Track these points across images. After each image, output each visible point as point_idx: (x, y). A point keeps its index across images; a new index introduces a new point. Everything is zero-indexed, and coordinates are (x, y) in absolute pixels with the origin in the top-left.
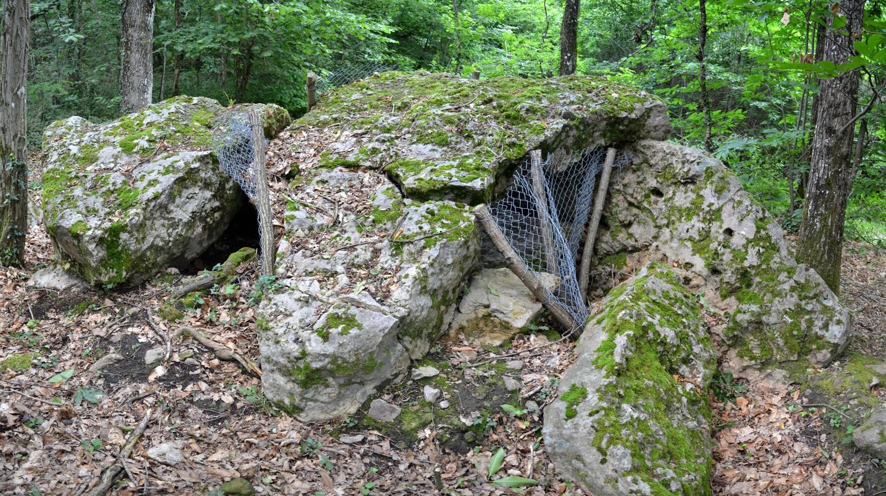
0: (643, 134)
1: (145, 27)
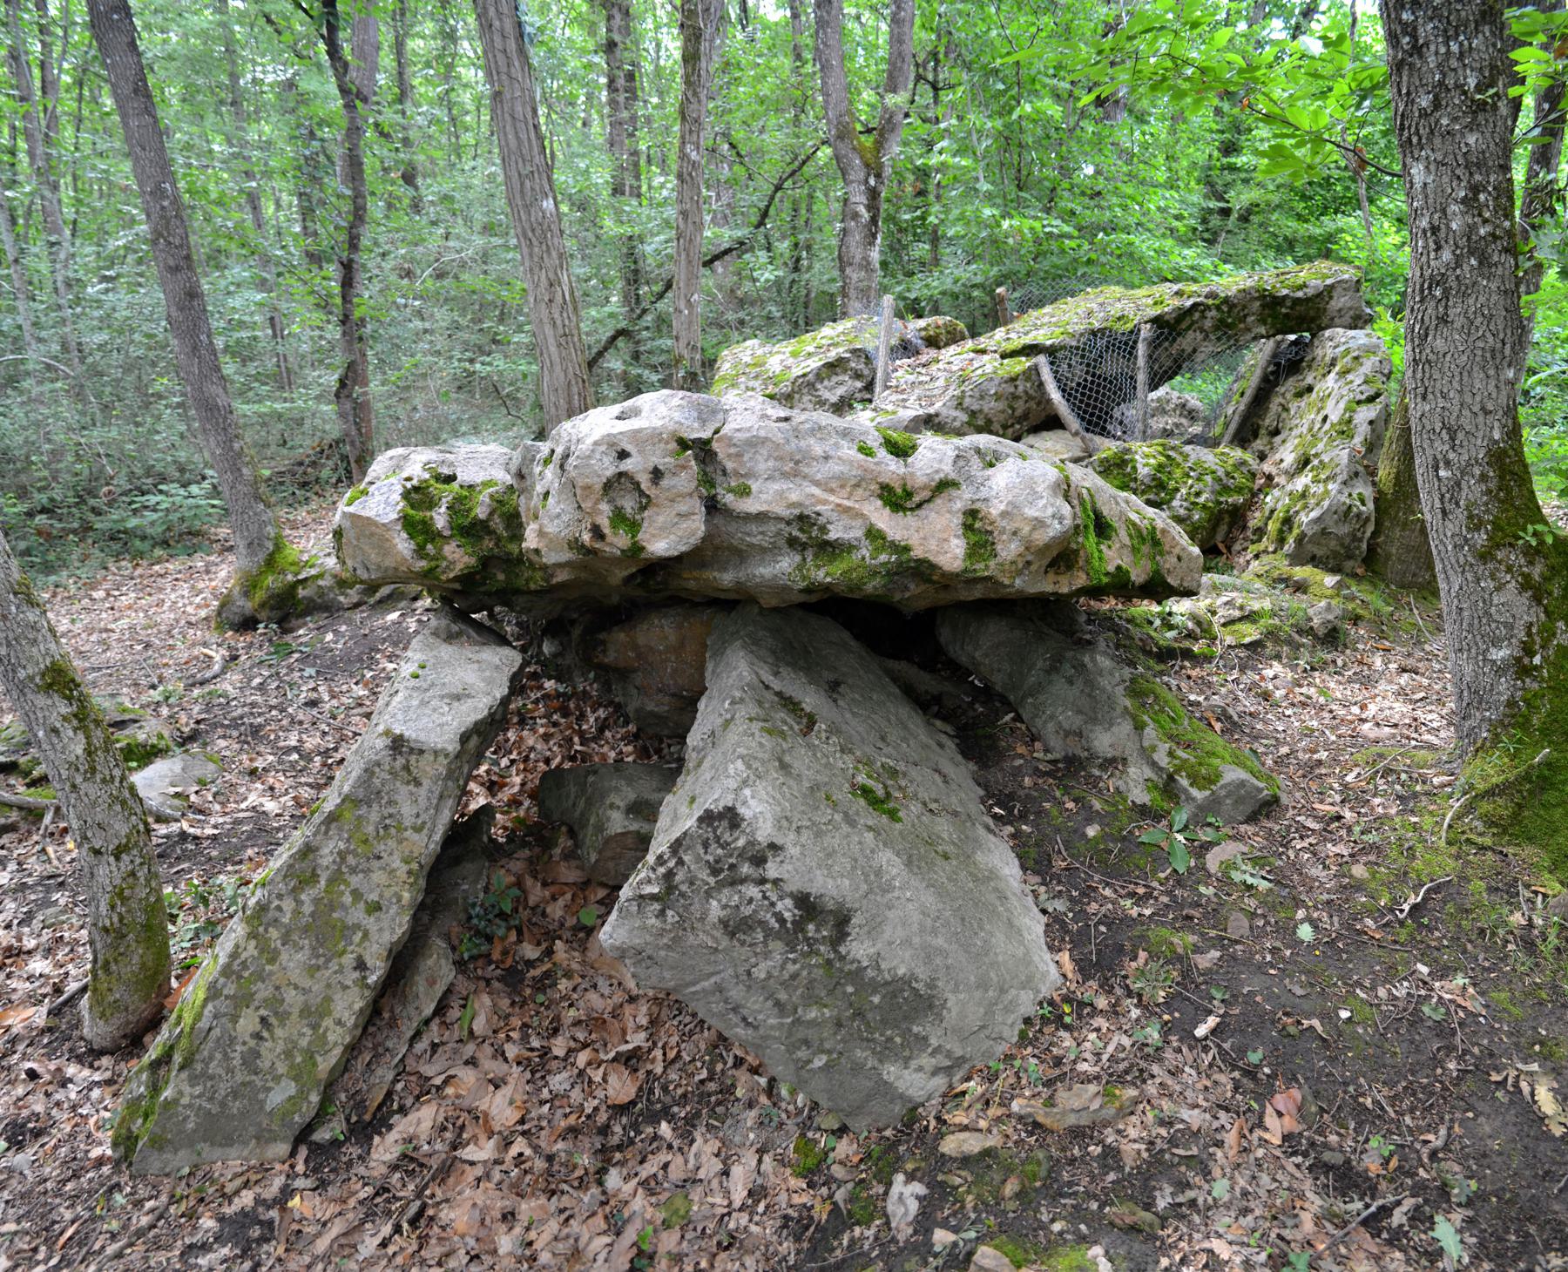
0: (1325, 321)
1: (866, 265)
